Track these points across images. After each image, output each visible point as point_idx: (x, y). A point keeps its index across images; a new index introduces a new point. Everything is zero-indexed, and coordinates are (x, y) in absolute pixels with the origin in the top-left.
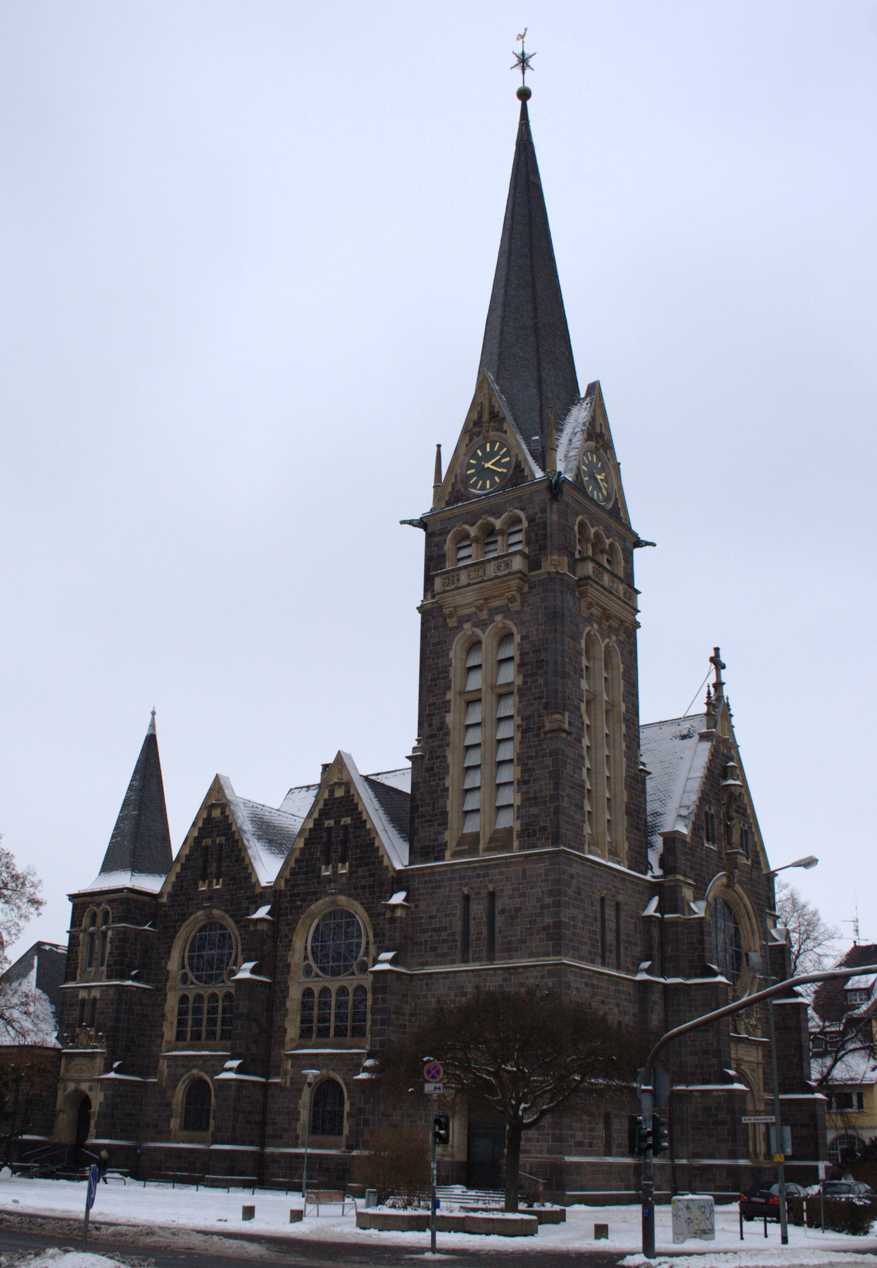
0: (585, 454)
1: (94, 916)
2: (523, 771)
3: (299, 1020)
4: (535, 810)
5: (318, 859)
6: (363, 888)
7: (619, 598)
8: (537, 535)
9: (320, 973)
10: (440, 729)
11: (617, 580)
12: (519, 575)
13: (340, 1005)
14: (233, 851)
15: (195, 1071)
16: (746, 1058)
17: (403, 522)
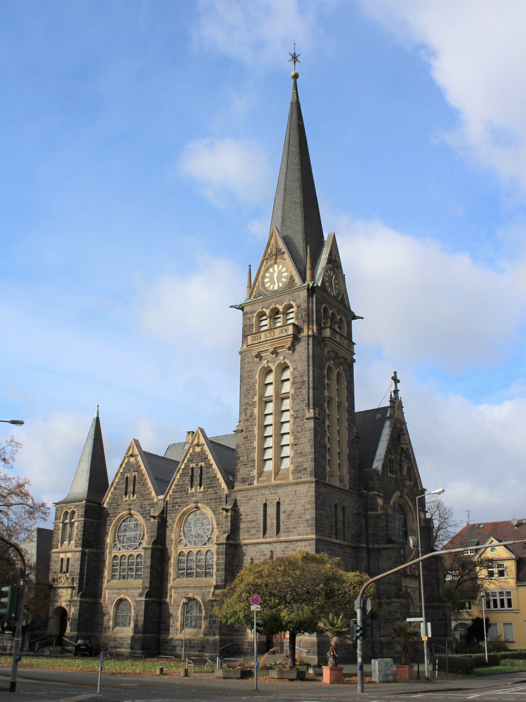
2: (294, 439)
4: (301, 459)
5: (187, 484)
6: (211, 499)
8: (302, 315)
10: (251, 416)
14: (141, 480)
16: (410, 585)
17: (231, 307)
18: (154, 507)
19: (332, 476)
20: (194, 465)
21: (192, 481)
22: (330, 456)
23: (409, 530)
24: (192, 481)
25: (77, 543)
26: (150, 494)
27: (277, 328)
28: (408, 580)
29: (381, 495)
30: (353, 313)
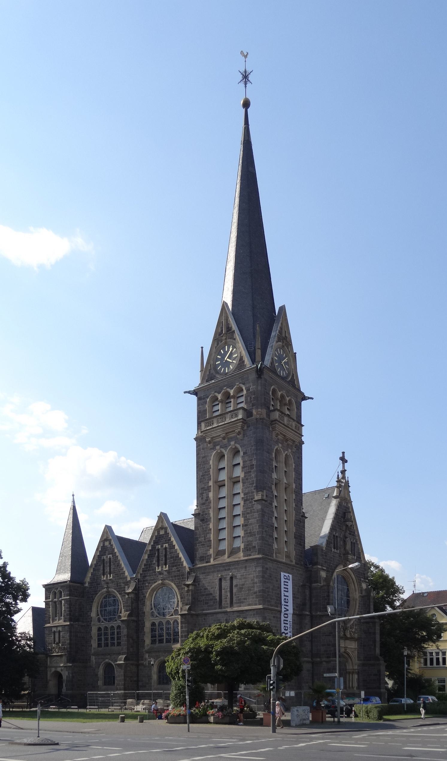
0: (276, 350)
1: (55, 593)
2: (245, 520)
3: (150, 637)
4: (250, 539)
5: (155, 564)
6: (175, 576)
7: (293, 430)
8: (251, 398)
9: (158, 615)
10: (207, 500)
11: (291, 420)
12: (241, 420)
13: (168, 629)
14: (116, 562)
15: (107, 660)
16: (349, 647)
17: (185, 392)
18: (128, 585)
19: (280, 553)
20: (159, 546)
21: (158, 561)
22: (277, 534)
23: (351, 599)
24: (158, 561)
25: (66, 618)
26: (124, 573)
27: (227, 413)
28: (348, 642)
29: (324, 568)
30: (303, 394)
